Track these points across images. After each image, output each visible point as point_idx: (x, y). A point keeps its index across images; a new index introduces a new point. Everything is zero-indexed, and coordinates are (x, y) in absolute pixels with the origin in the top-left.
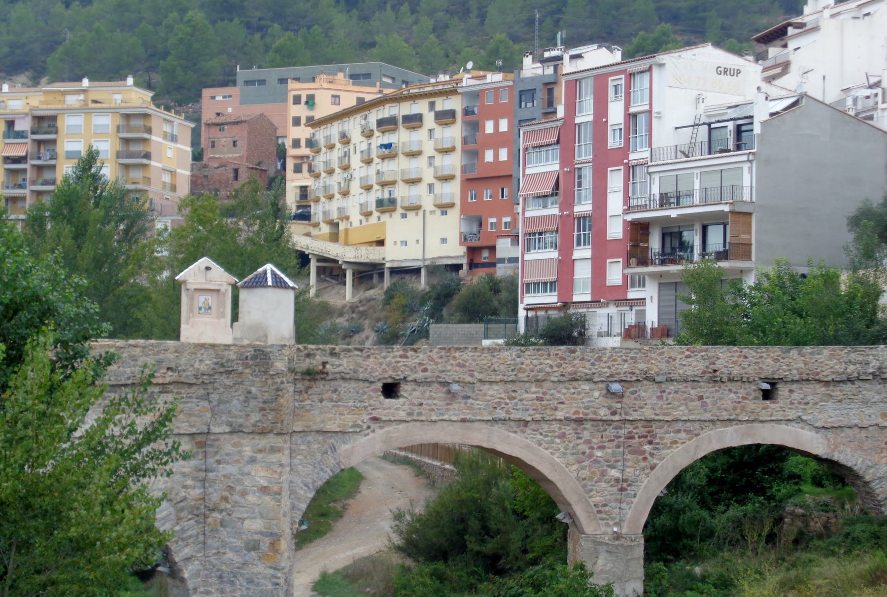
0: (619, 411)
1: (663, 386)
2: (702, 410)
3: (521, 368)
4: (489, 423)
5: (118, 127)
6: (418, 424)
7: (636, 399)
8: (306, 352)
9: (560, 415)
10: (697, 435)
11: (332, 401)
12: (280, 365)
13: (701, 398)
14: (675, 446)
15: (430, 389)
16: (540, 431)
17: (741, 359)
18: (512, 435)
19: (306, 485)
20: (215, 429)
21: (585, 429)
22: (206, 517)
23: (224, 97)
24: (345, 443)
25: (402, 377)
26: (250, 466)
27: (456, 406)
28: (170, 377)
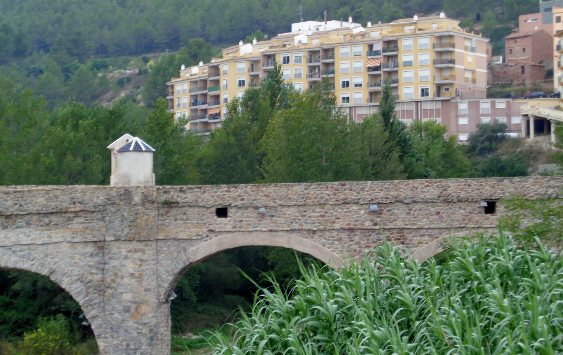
0: (379, 223)
1: (411, 206)
2: (439, 222)
3: (308, 197)
4: (289, 232)
5: (434, 44)
6: (240, 233)
7: (391, 215)
8: (164, 190)
9: (337, 226)
10: (437, 238)
11: (182, 220)
12: (137, 199)
13: (438, 213)
14: (421, 245)
15: (247, 211)
16: (324, 236)
17: (466, 187)
18: (305, 239)
19: (168, 272)
20: (108, 239)
21: (355, 235)
22: (105, 292)
23: (533, 20)
24: (192, 246)
25: (227, 204)
26: (125, 261)
27: (265, 221)
28: (78, 207)
